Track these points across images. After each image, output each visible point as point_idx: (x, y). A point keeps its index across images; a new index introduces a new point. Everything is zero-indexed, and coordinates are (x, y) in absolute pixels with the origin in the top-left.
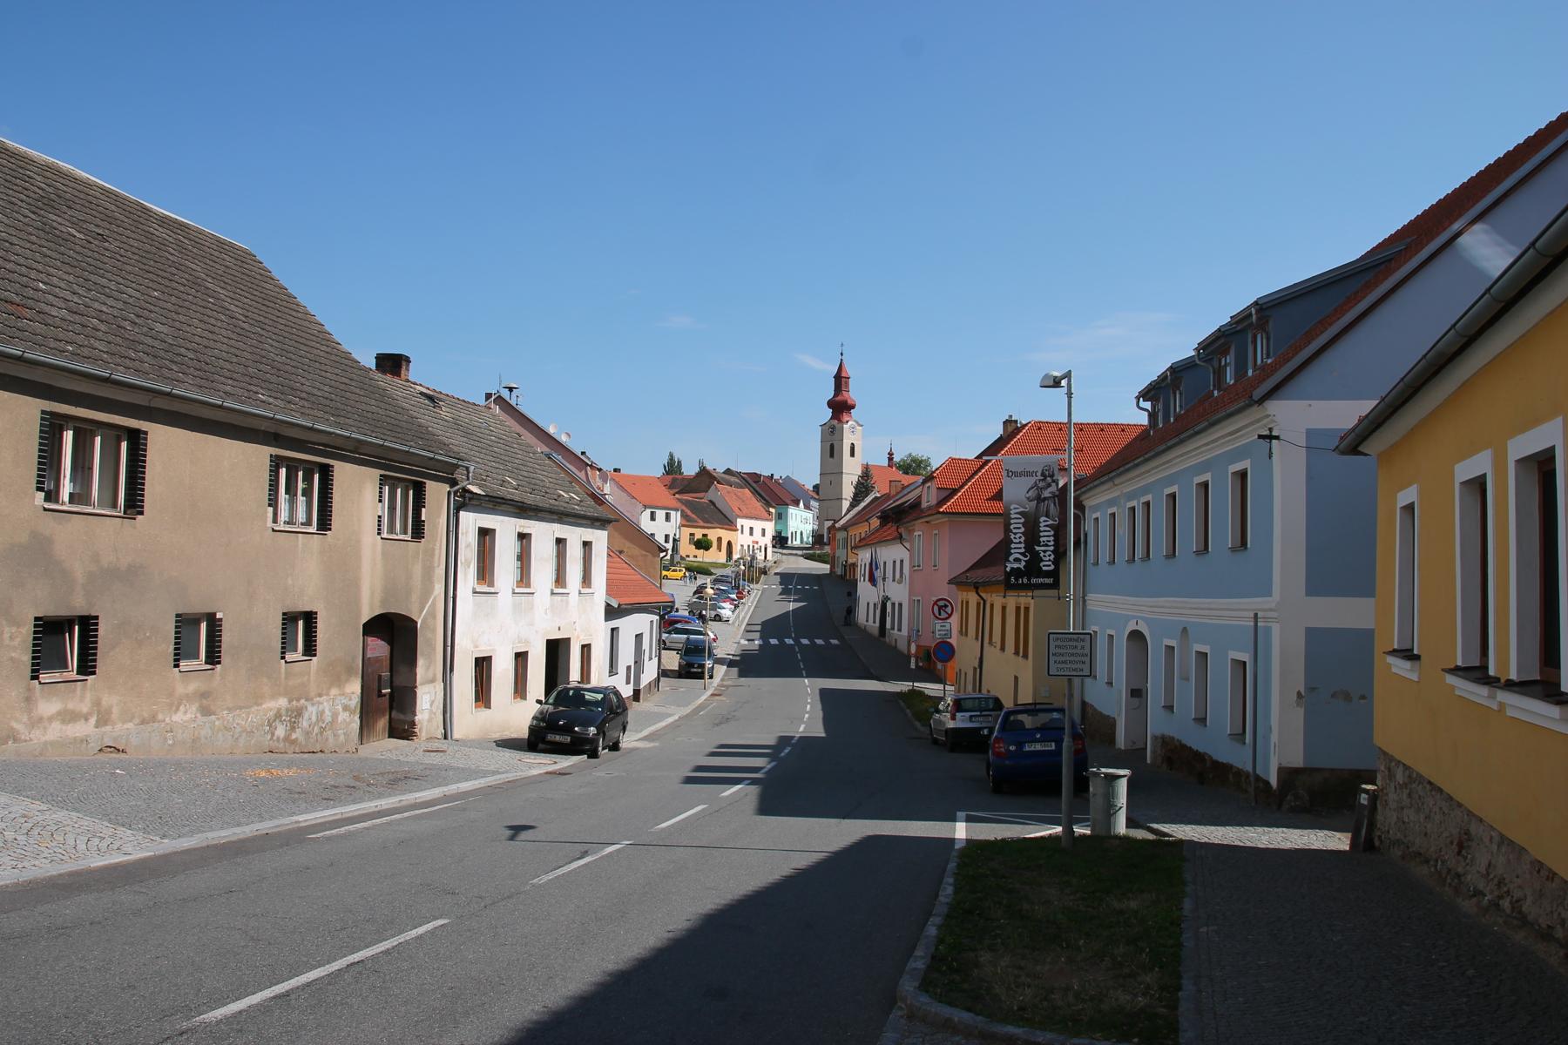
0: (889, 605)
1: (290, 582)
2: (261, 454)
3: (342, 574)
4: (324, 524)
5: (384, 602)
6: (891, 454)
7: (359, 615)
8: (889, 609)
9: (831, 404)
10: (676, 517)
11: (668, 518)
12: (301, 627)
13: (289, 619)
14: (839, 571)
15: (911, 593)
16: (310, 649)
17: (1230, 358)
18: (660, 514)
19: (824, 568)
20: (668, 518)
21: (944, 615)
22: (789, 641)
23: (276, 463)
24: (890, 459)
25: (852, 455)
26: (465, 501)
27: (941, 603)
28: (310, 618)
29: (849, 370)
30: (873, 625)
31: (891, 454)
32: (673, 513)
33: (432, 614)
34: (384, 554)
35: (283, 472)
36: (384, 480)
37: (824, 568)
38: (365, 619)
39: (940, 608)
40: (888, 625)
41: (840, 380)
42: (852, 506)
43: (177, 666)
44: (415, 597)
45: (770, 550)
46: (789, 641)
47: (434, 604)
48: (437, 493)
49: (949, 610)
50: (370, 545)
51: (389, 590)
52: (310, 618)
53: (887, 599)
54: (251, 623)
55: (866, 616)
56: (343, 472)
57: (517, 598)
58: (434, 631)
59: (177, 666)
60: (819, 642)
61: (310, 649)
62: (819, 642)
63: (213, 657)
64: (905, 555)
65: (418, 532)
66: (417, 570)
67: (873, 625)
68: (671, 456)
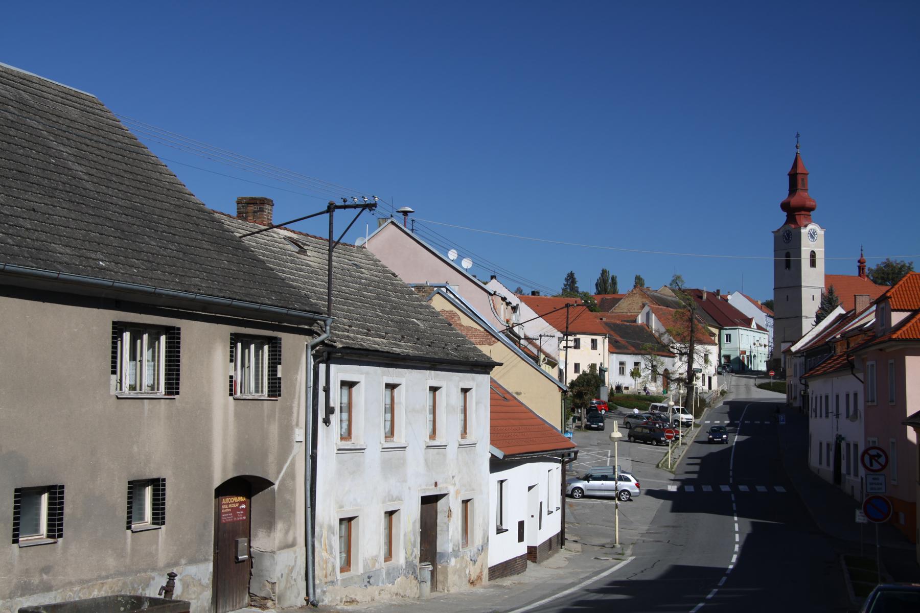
0: (843, 445)
1: (135, 449)
2: (101, 320)
3: (192, 438)
4: (173, 387)
5: (237, 464)
7: (210, 479)
9: (785, 206)
10: (603, 343)
11: (594, 344)
12: (146, 492)
13: (135, 487)
16: (159, 517)
19: (781, 397)
20: (594, 344)
22: (725, 488)
23: (118, 329)
24: (861, 268)
25: (813, 264)
26: (328, 354)
28: (158, 485)
29: (805, 165)
32: (599, 339)
33: (291, 475)
34: (237, 415)
35: (127, 336)
36: (235, 339)
37: (781, 397)
38: (217, 483)
39: (872, 457)
40: (844, 470)
41: (795, 180)
42: (819, 318)
43: (15, 541)
44: (272, 458)
46: (725, 488)
47: (293, 464)
48: (296, 346)
49: (882, 460)
50: (222, 407)
51: (244, 450)
52: (158, 485)
54: (95, 489)
55: (819, 461)
56: (193, 332)
57: (388, 455)
58: (293, 492)
59: (15, 541)
60: (761, 489)
61: (159, 517)
62: (761, 489)
63: (56, 529)
64: (860, 388)
65: (275, 389)
66: (274, 430)
68: (604, 272)
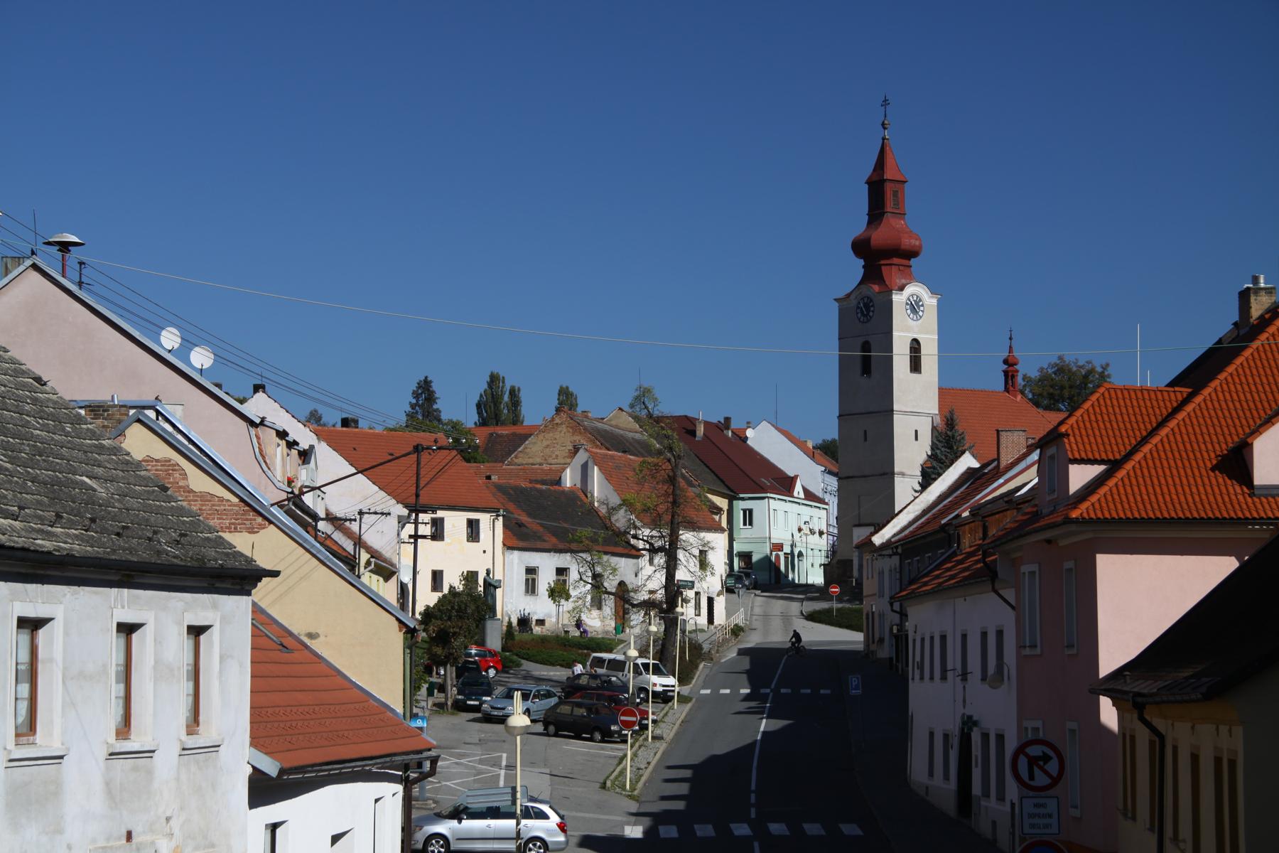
0: (976, 737)
6: (1009, 363)
8: (976, 750)
9: (861, 247)
11: (473, 527)
14: (885, 652)
15: (1021, 716)
17: (911, 502)
18: (455, 522)
21: (1041, 779)
22: (741, 830)
24: (1009, 376)
25: (916, 366)
27: (1035, 751)
29: (899, 164)
30: (943, 788)
31: (1009, 363)
32: (485, 519)
39: (1033, 761)
40: (976, 789)
41: (880, 193)
42: (928, 477)
45: (720, 605)
49: (1053, 767)
53: (969, 723)
55: (927, 770)
60: (812, 829)
62: (812, 829)
64: (1007, 619)
67: (943, 788)
68: (494, 379)
